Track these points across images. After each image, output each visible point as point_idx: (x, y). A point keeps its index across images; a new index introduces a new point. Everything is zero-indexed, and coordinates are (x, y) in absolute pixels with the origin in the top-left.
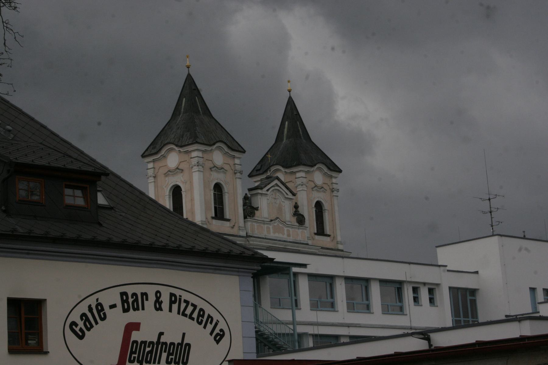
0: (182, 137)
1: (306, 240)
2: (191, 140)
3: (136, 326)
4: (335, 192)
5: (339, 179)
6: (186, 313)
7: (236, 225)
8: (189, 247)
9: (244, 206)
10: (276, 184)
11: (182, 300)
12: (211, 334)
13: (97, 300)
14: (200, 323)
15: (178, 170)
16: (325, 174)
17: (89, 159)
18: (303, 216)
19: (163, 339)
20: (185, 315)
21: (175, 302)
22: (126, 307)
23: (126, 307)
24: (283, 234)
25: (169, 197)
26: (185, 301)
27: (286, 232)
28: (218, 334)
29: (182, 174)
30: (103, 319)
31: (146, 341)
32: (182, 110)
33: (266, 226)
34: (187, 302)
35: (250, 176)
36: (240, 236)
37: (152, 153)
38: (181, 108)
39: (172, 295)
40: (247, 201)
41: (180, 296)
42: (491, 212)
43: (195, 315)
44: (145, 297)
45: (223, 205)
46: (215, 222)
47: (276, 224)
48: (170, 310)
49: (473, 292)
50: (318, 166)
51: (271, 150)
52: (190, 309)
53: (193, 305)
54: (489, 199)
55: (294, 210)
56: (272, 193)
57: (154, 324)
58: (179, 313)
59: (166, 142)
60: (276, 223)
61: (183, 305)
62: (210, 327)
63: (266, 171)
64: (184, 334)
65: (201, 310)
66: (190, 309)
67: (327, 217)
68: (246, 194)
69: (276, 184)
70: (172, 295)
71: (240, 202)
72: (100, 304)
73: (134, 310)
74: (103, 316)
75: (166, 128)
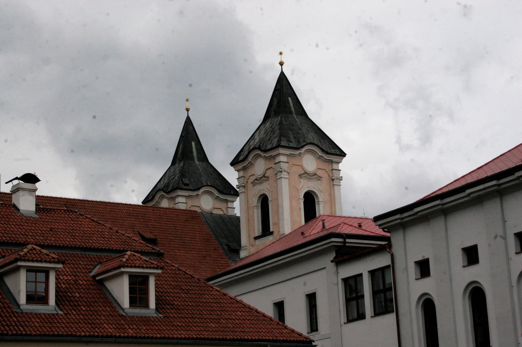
5: (344, 166)
15: (264, 178)
16: (320, 157)
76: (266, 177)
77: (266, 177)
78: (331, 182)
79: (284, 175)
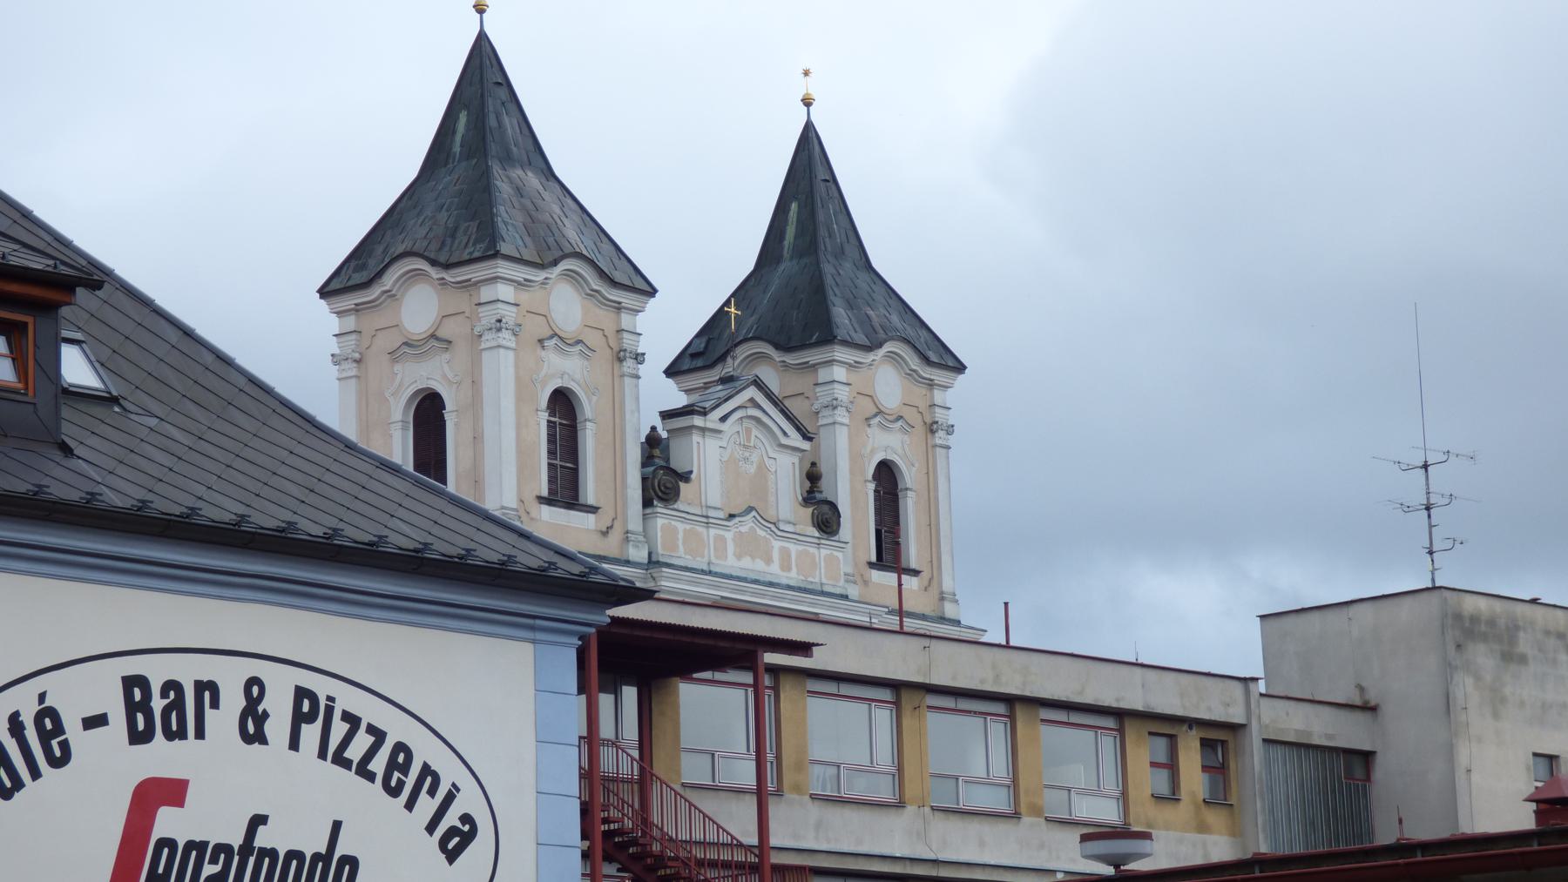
0: (453, 236)
1: (842, 583)
2: (481, 246)
3: (171, 791)
4: (941, 434)
5: (957, 396)
6: (347, 754)
7: (617, 524)
8: (367, 538)
9: (644, 465)
10: (752, 400)
11: (337, 715)
12: (431, 828)
13: (42, 697)
14: (394, 792)
15: (437, 340)
16: (912, 374)
17: (48, 238)
18: (833, 506)
19: (263, 839)
20: (346, 764)
21: (311, 718)
22: (141, 726)
23: (141, 726)
24: (769, 561)
25: (404, 429)
26: (347, 717)
27: (776, 555)
28: (452, 832)
29: (447, 356)
30: (60, 760)
31: (206, 844)
32: (457, 149)
33: (713, 532)
34: (352, 720)
35: (672, 371)
36: (627, 563)
37: (351, 283)
38: (453, 141)
39: (301, 693)
40: (657, 452)
41: (330, 699)
42: (1428, 509)
43: (378, 765)
44: (207, 695)
45: (575, 460)
46: (548, 513)
47: (744, 529)
48: (294, 744)
49: (1367, 757)
50: (888, 347)
51: (742, 293)
52: (362, 742)
53: (371, 729)
54: (1425, 467)
55: (808, 484)
56: (737, 428)
57: (229, 787)
58: (322, 754)
59: (401, 249)
60: (747, 524)
61: (339, 729)
62: (427, 806)
63: (722, 359)
64: (337, 826)
65: (400, 747)
66: (362, 742)
67: (911, 508)
68: (653, 429)
69: (752, 400)
70: (301, 693)
71: (634, 455)
72: (52, 713)
73: (170, 735)
74: (58, 753)
75: (401, 205)
76: (438, 339)
77: (438, 339)
78: (617, 365)
79: (841, 416)
